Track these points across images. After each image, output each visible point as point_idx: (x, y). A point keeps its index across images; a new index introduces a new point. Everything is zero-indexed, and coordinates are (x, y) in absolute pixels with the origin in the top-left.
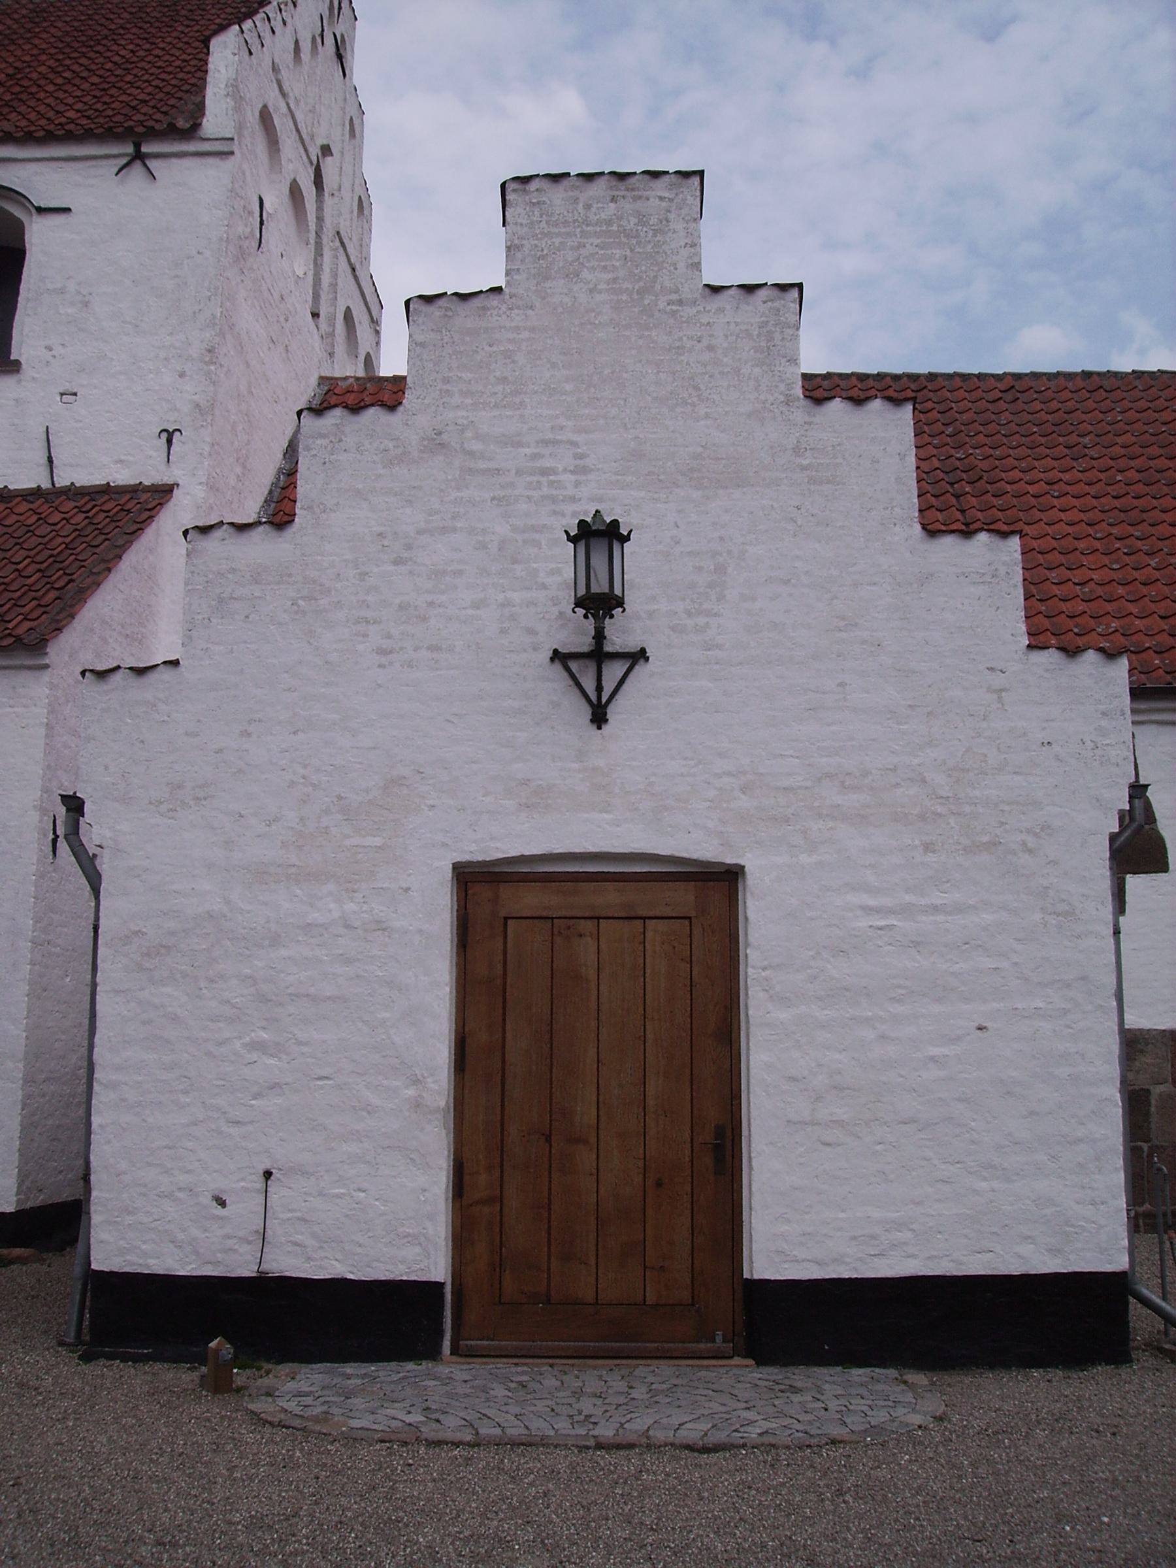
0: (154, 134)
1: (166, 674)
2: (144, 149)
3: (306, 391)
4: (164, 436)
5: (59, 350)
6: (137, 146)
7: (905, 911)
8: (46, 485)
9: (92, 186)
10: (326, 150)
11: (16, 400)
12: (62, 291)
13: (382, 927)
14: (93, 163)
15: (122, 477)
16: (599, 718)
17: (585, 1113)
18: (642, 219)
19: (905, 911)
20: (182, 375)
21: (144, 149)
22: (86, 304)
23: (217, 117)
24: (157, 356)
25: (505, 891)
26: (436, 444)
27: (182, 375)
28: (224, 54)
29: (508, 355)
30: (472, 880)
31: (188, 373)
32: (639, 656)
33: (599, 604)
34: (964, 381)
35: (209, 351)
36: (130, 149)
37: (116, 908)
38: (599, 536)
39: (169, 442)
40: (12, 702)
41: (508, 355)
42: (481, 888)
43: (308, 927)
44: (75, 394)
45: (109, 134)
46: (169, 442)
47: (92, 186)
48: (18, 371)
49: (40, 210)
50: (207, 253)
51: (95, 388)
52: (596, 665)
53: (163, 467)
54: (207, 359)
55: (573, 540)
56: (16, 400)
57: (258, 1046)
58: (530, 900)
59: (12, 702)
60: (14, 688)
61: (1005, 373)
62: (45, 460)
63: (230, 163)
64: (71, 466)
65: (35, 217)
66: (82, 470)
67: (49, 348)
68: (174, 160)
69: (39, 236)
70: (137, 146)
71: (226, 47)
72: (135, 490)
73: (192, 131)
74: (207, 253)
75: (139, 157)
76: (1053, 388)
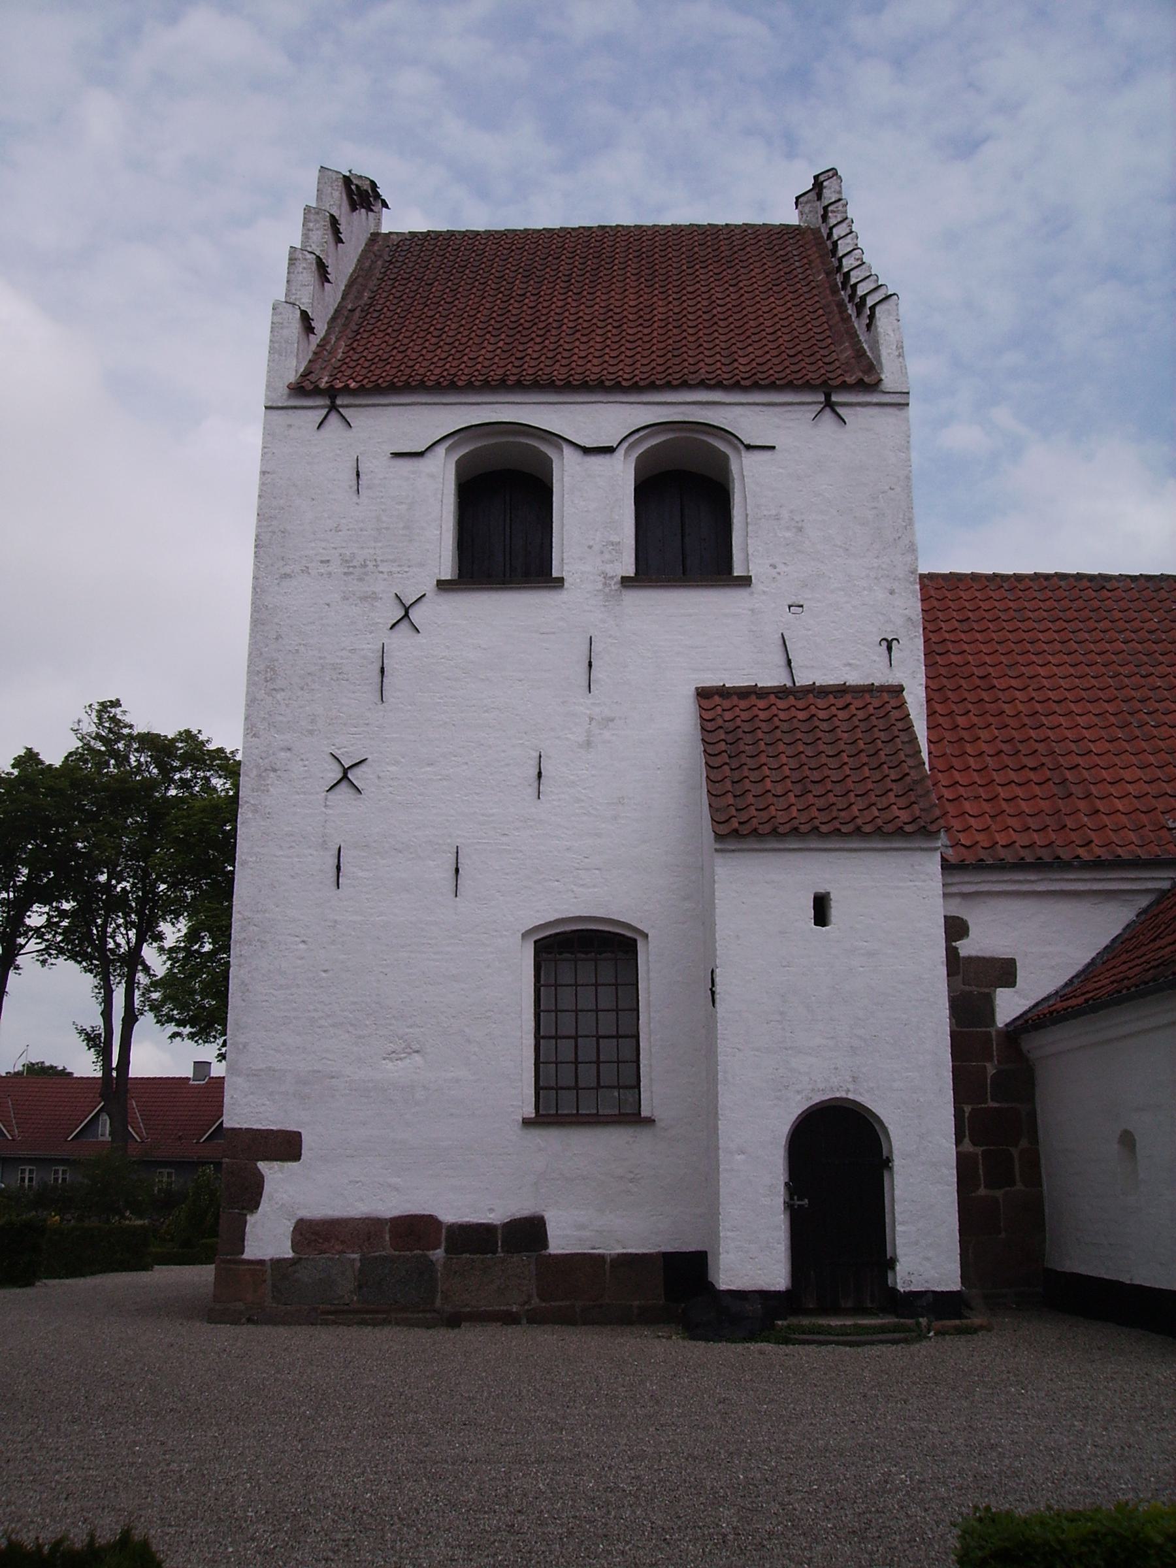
0: (845, 387)
2: (834, 399)
4: (884, 644)
5: (781, 568)
6: (828, 396)
8: (789, 684)
9: (789, 428)
11: (752, 610)
14: (789, 408)
20: (892, 592)
21: (834, 399)
22: (800, 529)
24: (868, 576)
27: (892, 592)
36: (328, 402)
39: (889, 649)
40: (911, 877)
46: (889, 649)
47: (789, 428)
49: (749, 447)
50: (898, 489)
53: (887, 671)
56: (752, 610)
59: (911, 877)
65: (744, 453)
67: (774, 566)
68: (858, 409)
70: (828, 396)
71: (890, 314)
74: (898, 489)
75: (333, 408)
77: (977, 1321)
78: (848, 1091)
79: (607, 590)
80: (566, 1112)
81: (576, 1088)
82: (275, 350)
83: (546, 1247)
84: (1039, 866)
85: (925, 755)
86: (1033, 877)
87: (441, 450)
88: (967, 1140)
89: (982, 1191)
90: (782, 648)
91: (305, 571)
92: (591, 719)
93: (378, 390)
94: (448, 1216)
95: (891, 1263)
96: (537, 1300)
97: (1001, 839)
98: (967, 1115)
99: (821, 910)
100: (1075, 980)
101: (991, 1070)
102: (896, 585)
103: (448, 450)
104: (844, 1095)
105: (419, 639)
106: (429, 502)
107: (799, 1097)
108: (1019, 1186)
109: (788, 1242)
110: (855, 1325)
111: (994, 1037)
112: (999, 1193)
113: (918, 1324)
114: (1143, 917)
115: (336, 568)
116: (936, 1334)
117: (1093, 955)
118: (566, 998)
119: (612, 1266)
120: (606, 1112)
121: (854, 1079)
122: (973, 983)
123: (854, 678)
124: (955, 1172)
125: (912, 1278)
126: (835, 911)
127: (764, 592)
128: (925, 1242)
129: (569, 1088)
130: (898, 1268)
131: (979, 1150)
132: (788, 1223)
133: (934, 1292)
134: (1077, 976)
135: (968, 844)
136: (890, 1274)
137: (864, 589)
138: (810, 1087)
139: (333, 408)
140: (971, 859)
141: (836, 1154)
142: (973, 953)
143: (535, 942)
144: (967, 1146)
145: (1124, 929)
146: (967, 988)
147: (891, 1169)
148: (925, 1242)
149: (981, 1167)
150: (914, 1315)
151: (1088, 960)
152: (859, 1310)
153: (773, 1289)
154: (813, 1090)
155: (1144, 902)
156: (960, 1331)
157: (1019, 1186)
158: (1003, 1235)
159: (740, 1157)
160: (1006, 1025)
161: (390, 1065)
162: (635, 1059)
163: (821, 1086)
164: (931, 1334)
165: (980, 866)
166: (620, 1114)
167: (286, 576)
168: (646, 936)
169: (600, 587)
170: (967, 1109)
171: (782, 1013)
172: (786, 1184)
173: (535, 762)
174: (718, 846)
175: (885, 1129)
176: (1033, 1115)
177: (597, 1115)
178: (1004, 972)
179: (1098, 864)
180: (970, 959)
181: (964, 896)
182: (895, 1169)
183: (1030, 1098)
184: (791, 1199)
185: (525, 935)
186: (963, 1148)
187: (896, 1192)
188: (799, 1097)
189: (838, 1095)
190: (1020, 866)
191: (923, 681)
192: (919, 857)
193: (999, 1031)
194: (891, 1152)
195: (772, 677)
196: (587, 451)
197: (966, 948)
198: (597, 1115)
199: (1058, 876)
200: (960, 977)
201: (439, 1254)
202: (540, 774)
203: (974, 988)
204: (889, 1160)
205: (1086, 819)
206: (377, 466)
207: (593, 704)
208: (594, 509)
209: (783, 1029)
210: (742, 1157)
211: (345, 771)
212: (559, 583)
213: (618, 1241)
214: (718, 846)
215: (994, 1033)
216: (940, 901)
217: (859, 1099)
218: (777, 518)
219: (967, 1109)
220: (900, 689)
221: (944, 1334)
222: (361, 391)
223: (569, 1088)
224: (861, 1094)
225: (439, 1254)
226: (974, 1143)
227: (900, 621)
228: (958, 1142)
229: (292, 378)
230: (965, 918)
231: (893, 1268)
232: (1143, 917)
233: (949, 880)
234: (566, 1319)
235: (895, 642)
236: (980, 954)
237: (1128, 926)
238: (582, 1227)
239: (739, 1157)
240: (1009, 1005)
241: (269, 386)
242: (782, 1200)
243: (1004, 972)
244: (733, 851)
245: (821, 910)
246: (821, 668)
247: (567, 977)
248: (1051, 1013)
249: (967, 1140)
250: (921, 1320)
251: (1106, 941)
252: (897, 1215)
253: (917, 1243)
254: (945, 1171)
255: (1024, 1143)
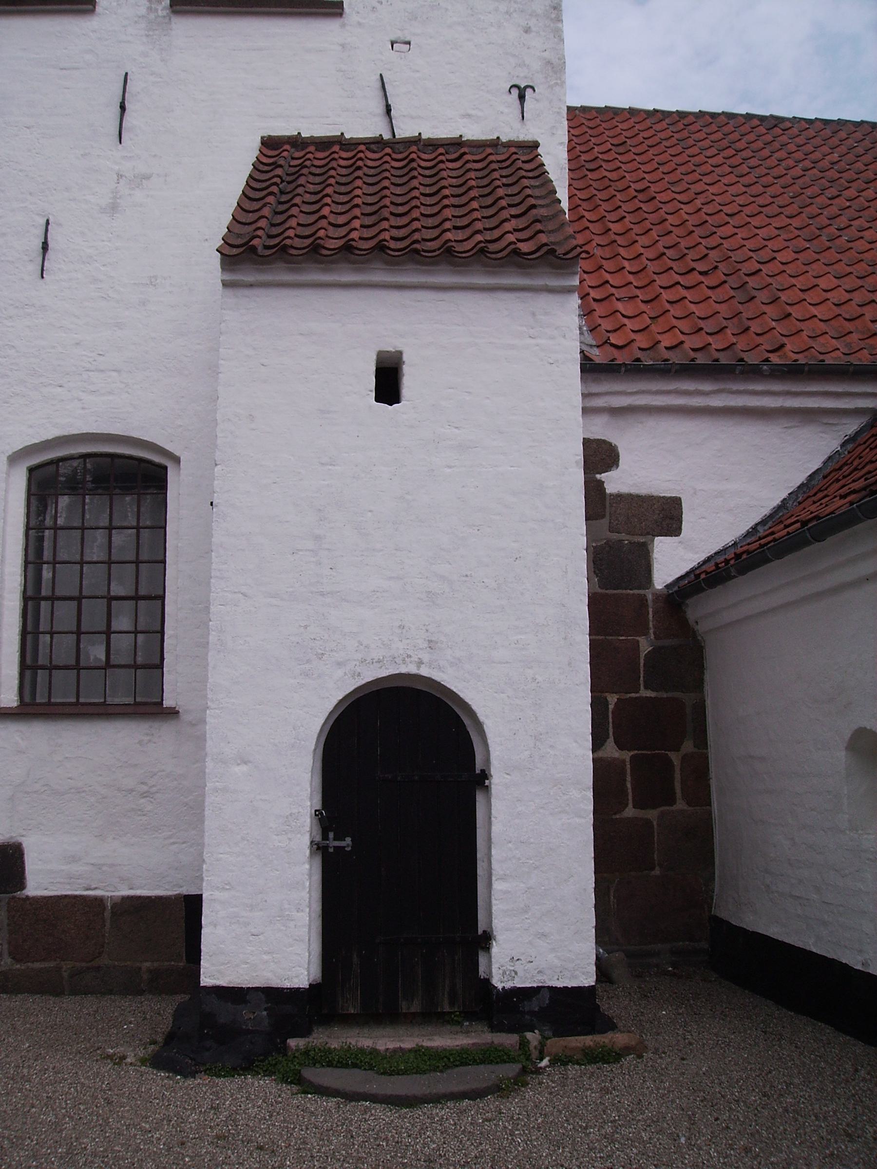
4: (515, 92)
8: (387, 136)
11: (343, 46)
20: (527, 30)
31: (534, 29)
34: (825, 124)
35: (555, 8)
39: (522, 97)
44: (409, 43)
46: (522, 97)
48: (340, 15)
51: (431, 37)
54: (553, 16)
56: (343, 46)
60: (534, 314)
61: (862, 121)
62: (381, 109)
64: (412, 118)
76: (845, 260)
77: (619, 1039)
78: (420, 663)
79: (152, 16)
80: (58, 700)
81: (77, 667)
83: (22, 885)
84: (714, 371)
85: (563, 194)
86: (706, 387)
88: (610, 743)
89: (630, 812)
90: (381, 93)
92: (120, 176)
95: (486, 940)
96: (9, 960)
97: (666, 341)
98: (611, 707)
99: (388, 383)
100: (759, 528)
101: (645, 646)
102: (532, 23)
104: (412, 669)
107: (340, 673)
108: (680, 805)
109: (317, 907)
110: (417, 1051)
111: (650, 603)
112: (652, 815)
113: (524, 1044)
114: (850, 447)
116: (552, 1063)
117: (784, 495)
119: (114, 913)
120: (117, 701)
121: (431, 645)
122: (621, 530)
123: (473, 132)
124: (590, 794)
125: (518, 967)
126: (409, 384)
127: (360, 24)
128: (540, 911)
129: (66, 668)
130: (495, 949)
131: (627, 755)
132: (317, 877)
133: (550, 988)
134: (763, 522)
135: (620, 343)
136: (482, 959)
137: (492, 25)
138: (359, 656)
140: (622, 358)
141: (398, 763)
142: (625, 489)
143: (31, 470)
144: (611, 750)
145: (825, 463)
146: (615, 536)
147: (487, 789)
148: (540, 911)
149: (629, 778)
150: (518, 1028)
151: (777, 502)
152: (431, 1016)
153: (287, 984)
154: (363, 661)
155: (852, 426)
156: (592, 1057)
157: (680, 805)
158: (657, 872)
159: (240, 770)
160: (668, 587)
162: (159, 629)
163: (376, 654)
164: (545, 1062)
165: (636, 370)
166: (136, 704)
168: (177, 460)
169: (143, 11)
170: (612, 699)
171: (318, 538)
172: (317, 813)
173: (41, 232)
174: (228, 277)
175: (479, 725)
176: (700, 709)
177: (104, 704)
178: (666, 516)
179: (793, 372)
180: (619, 497)
181: (615, 412)
182: (494, 789)
183: (699, 685)
184: (325, 837)
185: (14, 459)
186: (604, 753)
187: (493, 828)
188: (340, 673)
189: (404, 670)
190: (690, 370)
191: (565, 139)
192: (544, 301)
193: (657, 596)
194: (487, 761)
195: (364, 125)
197: (615, 482)
198: (49, 704)
199: (741, 387)
200: (605, 522)
202: (45, 247)
203: (623, 536)
204: (485, 775)
205: (774, 323)
207: (124, 157)
209: (319, 563)
210: (244, 768)
213: (122, 879)
214: (228, 277)
215: (650, 597)
216: (580, 398)
217: (437, 676)
219: (612, 699)
220: (536, 145)
221: (565, 1064)
223: (66, 668)
224: (440, 668)
226: (621, 746)
227: (536, 65)
228: (597, 745)
230: (614, 441)
231: (487, 949)
232: (850, 447)
233: (595, 388)
234: (48, 986)
235: (529, 92)
236: (634, 491)
237: (830, 458)
238: (74, 859)
239: (237, 769)
240: (671, 560)
242: (306, 840)
243: (666, 516)
244: (251, 286)
245: (388, 383)
246: (427, 116)
248: (737, 556)
249: (610, 743)
250: (529, 1035)
251: (801, 478)
252: (495, 865)
253: (526, 909)
254: (575, 794)
255: (688, 746)
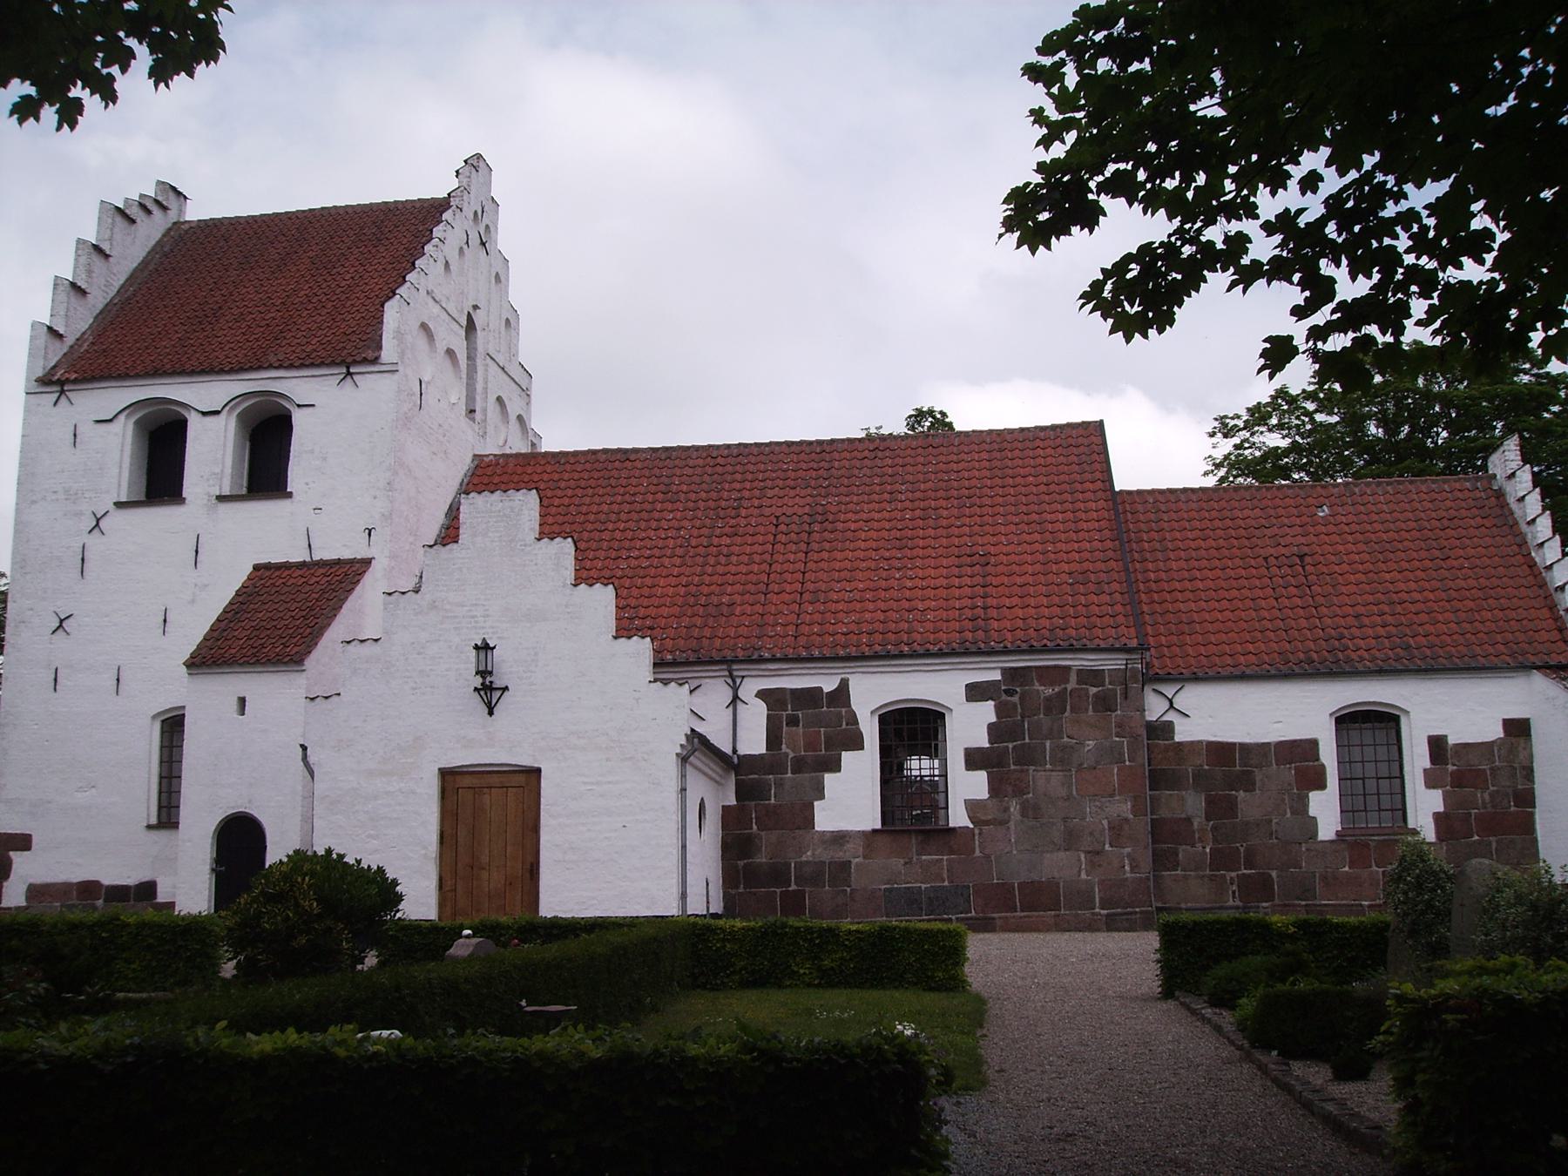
0: (355, 363)
1: (335, 698)
3: (460, 467)
7: (598, 783)
10: (476, 307)
12: (312, 452)
13: (413, 792)
15: (346, 554)
16: (491, 713)
17: (485, 859)
18: (512, 509)
19: (598, 783)
22: (325, 459)
23: (388, 352)
25: (458, 778)
26: (433, 606)
28: (391, 311)
29: (460, 569)
30: (446, 775)
32: (506, 689)
33: (483, 673)
37: (320, 786)
38: (484, 648)
41: (460, 569)
42: (450, 778)
43: (387, 793)
45: (333, 364)
52: (489, 692)
55: (476, 647)
57: (369, 836)
58: (467, 781)
63: (396, 376)
66: (327, 551)
69: (298, 418)
72: (352, 562)
73: (375, 361)
75: (349, 374)
82: (32, 355)
87: (122, 417)
91: (44, 498)
93: (93, 379)
94: (106, 882)
103: (128, 417)
105: (104, 539)
106: (115, 453)
115: (62, 496)
118: (1356, 751)
139: (62, 392)
161: (79, 795)
167: (34, 502)
185: (154, 717)
195: (299, 556)
196: (204, 414)
201: (100, 902)
206: (87, 429)
208: (212, 450)
211: (62, 621)
212: (290, 495)
218: (312, 452)
222: (75, 381)
225: (100, 902)
229: (40, 373)
241: (28, 379)
247: (1368, 739)
